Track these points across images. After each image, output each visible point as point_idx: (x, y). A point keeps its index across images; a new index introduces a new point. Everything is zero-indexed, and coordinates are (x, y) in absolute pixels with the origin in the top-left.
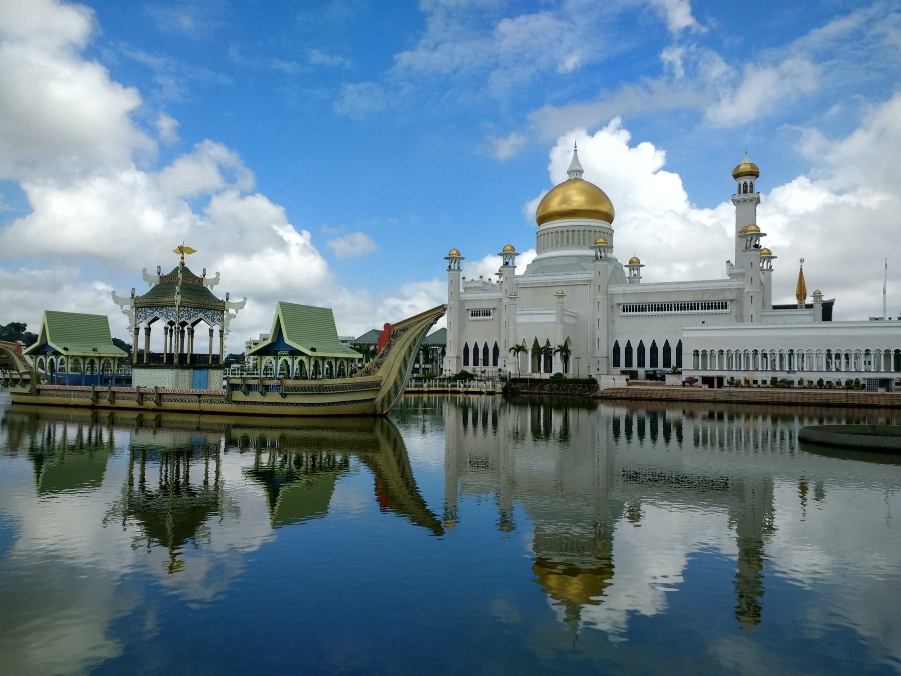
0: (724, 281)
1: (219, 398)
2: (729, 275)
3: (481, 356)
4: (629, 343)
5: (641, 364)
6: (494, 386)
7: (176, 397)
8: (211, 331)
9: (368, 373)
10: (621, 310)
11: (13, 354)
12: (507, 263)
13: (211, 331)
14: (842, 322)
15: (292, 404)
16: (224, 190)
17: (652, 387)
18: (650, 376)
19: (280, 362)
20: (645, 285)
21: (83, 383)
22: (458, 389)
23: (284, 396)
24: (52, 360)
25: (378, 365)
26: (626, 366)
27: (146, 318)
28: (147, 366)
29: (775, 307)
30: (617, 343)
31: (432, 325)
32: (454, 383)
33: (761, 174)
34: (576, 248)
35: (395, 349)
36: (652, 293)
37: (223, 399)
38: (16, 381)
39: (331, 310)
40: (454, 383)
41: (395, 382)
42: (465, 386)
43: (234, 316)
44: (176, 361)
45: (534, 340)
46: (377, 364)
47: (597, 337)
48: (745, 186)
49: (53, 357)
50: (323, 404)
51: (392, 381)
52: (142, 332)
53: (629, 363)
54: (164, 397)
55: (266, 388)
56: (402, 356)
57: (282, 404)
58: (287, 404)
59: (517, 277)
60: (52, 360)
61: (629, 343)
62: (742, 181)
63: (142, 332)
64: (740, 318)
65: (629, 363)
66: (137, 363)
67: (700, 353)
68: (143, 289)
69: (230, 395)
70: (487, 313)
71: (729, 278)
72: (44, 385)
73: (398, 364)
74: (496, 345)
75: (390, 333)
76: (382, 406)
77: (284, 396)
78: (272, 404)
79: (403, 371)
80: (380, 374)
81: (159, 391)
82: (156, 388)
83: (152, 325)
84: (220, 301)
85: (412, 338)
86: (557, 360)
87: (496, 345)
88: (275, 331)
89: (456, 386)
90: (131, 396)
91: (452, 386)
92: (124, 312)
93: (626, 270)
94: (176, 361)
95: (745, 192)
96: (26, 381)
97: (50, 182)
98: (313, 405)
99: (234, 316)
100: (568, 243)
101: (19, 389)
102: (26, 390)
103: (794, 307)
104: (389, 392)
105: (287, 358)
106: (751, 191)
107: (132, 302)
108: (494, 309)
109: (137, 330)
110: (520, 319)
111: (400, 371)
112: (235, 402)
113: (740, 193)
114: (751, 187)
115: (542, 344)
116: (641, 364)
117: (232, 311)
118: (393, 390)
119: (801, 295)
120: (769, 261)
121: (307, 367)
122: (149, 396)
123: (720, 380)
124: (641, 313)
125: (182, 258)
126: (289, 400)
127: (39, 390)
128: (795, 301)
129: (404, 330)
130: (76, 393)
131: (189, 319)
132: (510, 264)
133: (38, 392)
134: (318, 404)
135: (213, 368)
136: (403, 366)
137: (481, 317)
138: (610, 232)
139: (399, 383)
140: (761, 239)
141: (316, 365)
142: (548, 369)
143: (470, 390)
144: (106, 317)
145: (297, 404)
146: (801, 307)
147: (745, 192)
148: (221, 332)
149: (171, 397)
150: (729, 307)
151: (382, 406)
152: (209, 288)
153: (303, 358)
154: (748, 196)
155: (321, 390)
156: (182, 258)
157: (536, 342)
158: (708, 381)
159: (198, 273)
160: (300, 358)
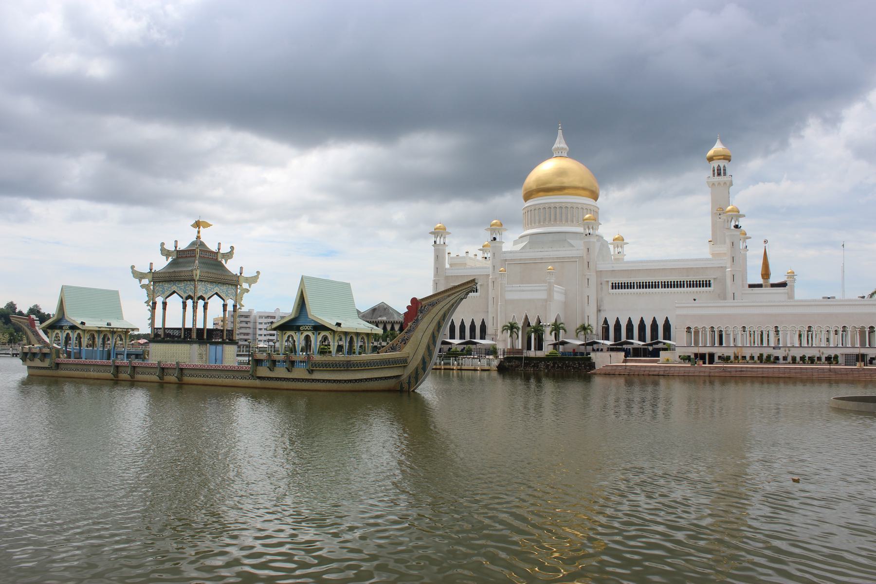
0: (707, 259)
1: (242, 374)
2: (712, 254)
4: (630, 321)
6: (489, 364)
7: (198, 372)
9: (393, 349)
11: (26, 328)
12: (495, 239)
13: (225, 306)
14: (801, 301)
15: (318, 380)
20: (628, 262)
22: (451, 367)
23: (311, 372)
24: (68, 334)
25: (405, 341)
27: (163, 293)
28: (163, 341)
29: (751, 286)
31: (462, 299)
32: (446, 361)
33: (732, 159)
34: (553, 225)
35: (422, 325)
36: (654, 270)
37: (246, 374)
38: (34, 355)
39: (117, 292)
40: (446, 361)
42: (458, 365)
43: (247, 291)
45: (524, 317)
46: (403, 340)
48: (719, 170)
49: (69, 332)
50: (350, 381)
51: (420, 357)
52: (159, 306)
54: (185, 372)
55: (274, 362)
57: (308, 380)
58: (313, 380)
59: (505, 252)
60: (68, 334)
62: (715, 164)
63: (159, 306)
64: (723, 296)
66: (185, 338)
67: (693, 330)
68: (161, 263)
69: (255, 371)
71: (710, 257)
72: (63, 358)
73: (425, 341)
74: (483, 322)
75: (417, 308)
76: (409, 383)
77: (311, 372)
78: (298, 380)
79: (432, 347)
80: (406, 351)
81: (162, 366)
82: (159, 363)
83: (168, 300)
84: (233, 276)
85: (441, 313)
87: (483, 322)
89: (449, 364)
90: (152, 371)
91: (445, 364)
92: (143, 286)
93: (611, 247)
94: (194, 335)
95: (719, 174)
96: (45, 356)
99: (247, 291)
100: (555, 220)
101: (37, 363)
102: (46, 364)
103: (760, 286)
104: (417, 369)
105: (310, 333)
106: (725, 174)
107: (151, 276)
109: (154, 304)
110: (509, 296)
111: (428, 347)
112: (259, 378)
113: (714, 174)
114: (725, 170)
115: (533, 323)
117: (245, 286)
119: (766, 274)
120: (744, 241)
122: (170, 371)
123: (712, 356)
125: (199, 232)
126: (316, 376)
127: (58, 365)
128: (760, 281)
129: (433, 305)
130: (96, 368)
131: (206, 293)
132: (498, 240)
133: (58, 365)
134: (345, 381)
135: (227, 343)
138: (596, 209)
139: (427, 359)
140: (740, 219)
141: (351, 342)
142: (540, 347)
143: (463, 367)
144: (349, 284)
145: (324, 380)
146: (766, 286)
147: (719, 174)
149: (193, 372)
151: (409, 383)
152: (223, 262)
154: (722, 178)
155: (348, 366)
156: (199, 232)
157: (526, 318)
159: (213, 248)
160: (323, 333)
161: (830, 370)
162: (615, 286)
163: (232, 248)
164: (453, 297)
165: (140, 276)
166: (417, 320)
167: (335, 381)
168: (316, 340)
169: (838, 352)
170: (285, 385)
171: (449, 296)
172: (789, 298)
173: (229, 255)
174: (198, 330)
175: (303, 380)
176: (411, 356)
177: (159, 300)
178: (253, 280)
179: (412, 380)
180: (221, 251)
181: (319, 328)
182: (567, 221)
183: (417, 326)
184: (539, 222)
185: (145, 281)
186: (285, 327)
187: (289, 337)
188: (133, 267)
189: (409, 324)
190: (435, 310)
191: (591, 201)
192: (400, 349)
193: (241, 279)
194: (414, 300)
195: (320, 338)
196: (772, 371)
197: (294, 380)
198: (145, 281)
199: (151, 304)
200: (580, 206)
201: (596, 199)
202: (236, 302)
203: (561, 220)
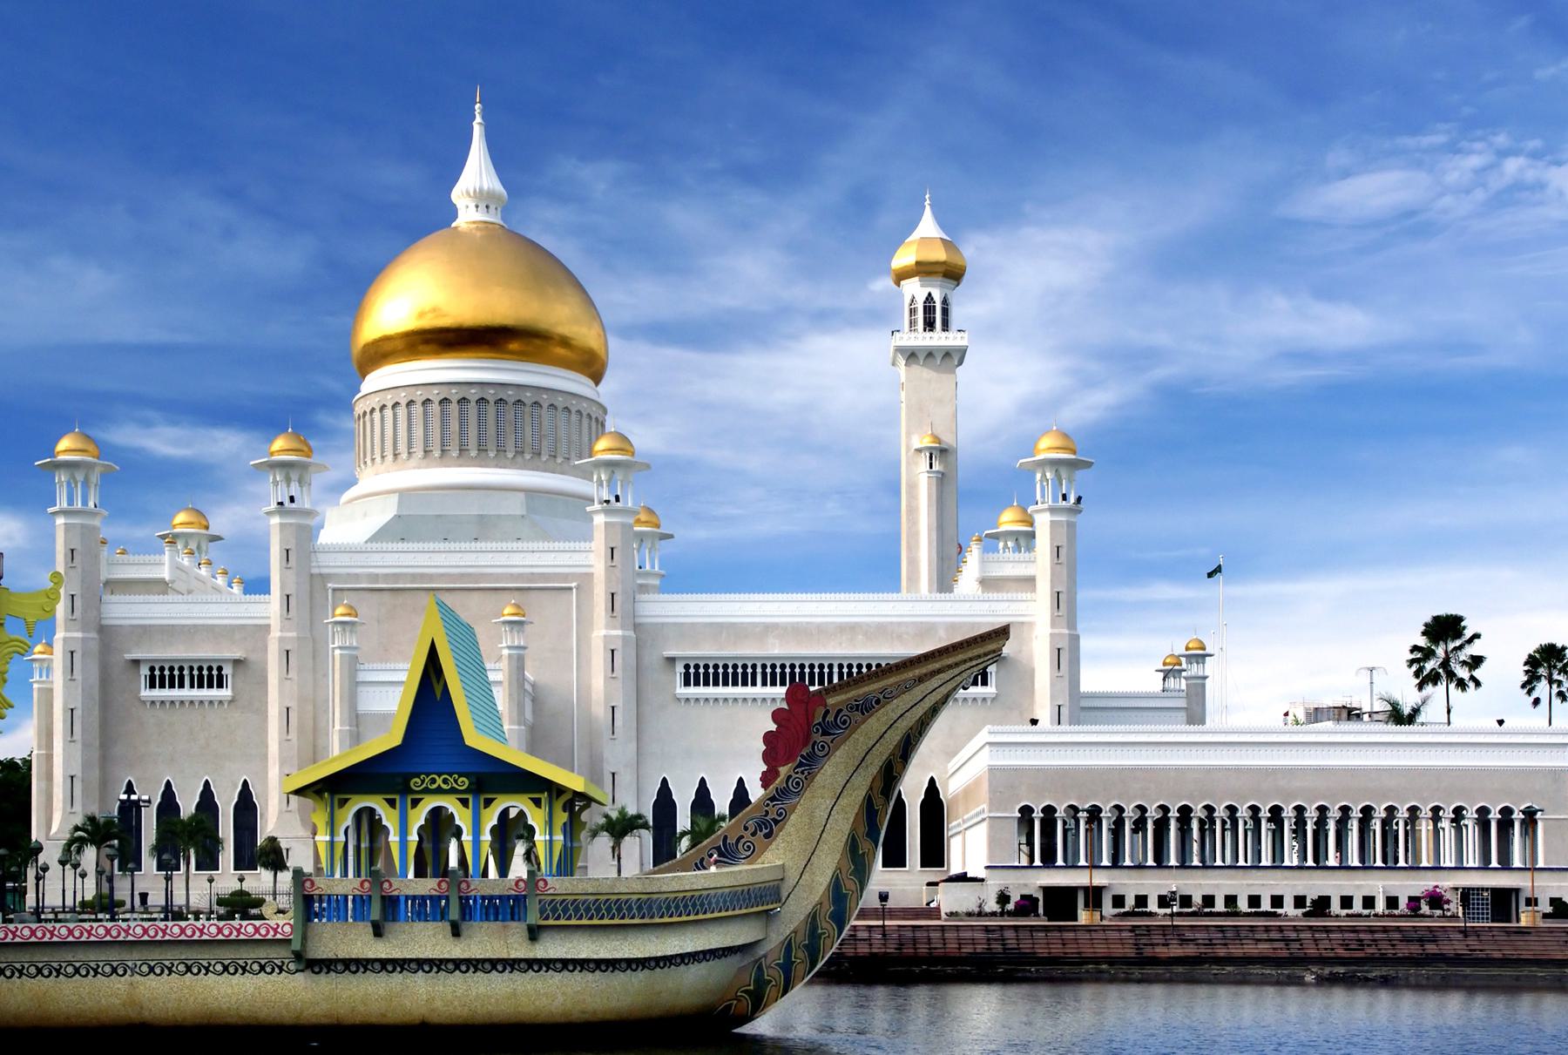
10: (679, 679)
19: (418, 817)
23: (534, 934)
30: (665, 787)
34: (512, 464)
35: (831, 772)
39: (1460, 619)
46: (761, 824)
47: (608, 769)
55: (391, 905)
70: (210, 676)
74: (245, 795)
75: (809, 717)
79: (865, 845)
85: (895, 737)
87: (245, 795)
97: (1338, 157)
104: (813, 918)
105: (451, 804)
108: (237, 663)
113: (912, 323)
114: (945, 312)
118: (829, 908)
121: (394, 838)
124: (740, 690)
129: (866, 707)
136: (862, 829)
137: (187, 693)
138: (595, 412)
139: (849, 885)
147: (929, 325)
150: (992, 679)
162: (698, 674)
164: (935, 682)
168: (474, 827)
169: (1446, 882)
171: (921, 680)
172: (1190, 721)
175: (511, 964)
176: (792, 877)
179: (799, 956)
181: (492, 777)
182: (520, 452)
183: (811, 777)
186: (378, 776)
187: (358, 815)
190: (874, 724)
191: (576, 383)
192: (753, 853)
200: (528, 397)
201: (597, 378)
203: (501, 450)
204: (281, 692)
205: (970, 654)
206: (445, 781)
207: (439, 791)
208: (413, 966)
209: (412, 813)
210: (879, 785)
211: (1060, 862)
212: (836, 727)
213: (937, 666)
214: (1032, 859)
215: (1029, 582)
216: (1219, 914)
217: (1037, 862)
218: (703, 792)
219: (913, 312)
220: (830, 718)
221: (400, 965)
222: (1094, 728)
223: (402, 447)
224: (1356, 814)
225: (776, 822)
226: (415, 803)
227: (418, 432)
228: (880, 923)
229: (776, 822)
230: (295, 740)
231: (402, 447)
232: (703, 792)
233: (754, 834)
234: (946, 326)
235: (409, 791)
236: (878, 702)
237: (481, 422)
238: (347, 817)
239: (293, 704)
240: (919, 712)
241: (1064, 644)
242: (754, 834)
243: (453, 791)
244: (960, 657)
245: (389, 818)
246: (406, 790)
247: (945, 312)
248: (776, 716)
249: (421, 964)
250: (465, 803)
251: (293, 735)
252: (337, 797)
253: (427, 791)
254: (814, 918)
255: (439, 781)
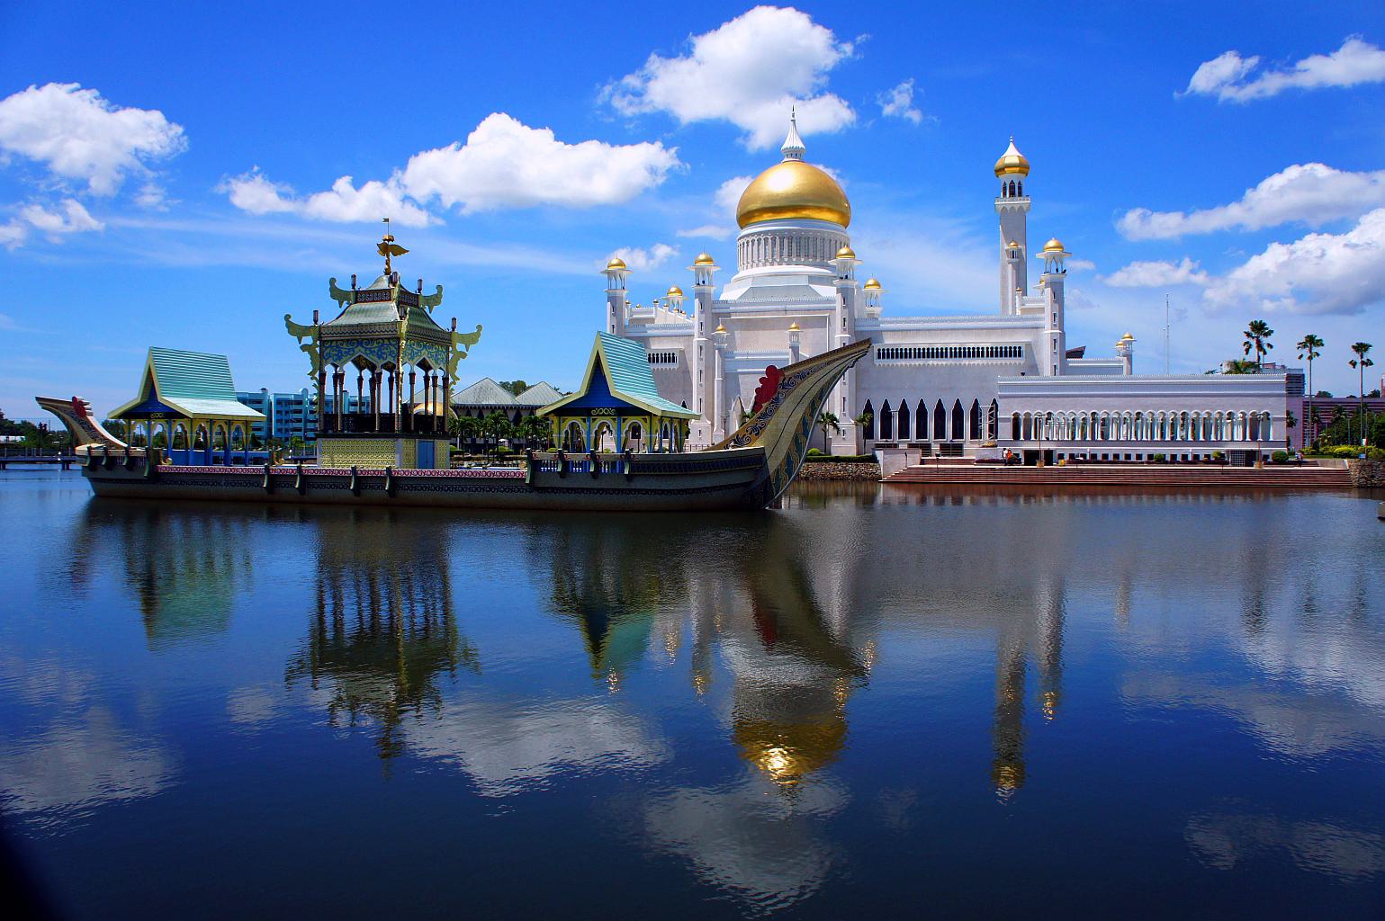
3: (896, 422)
4: (922, 405)
5: (940, 432)
8: (360, 380)
16: (1217, 86)
17: (950, 465)
18: (945, 449)
19: (595, 427)
21: (1043, 454)
26: (918, 437)
35: (786, 405)
41: (788, 456)
44: (397, 426)
46: (754, 429)
51: (782, 456)
53: (922, 432)
56: (798, 415)
57: (590, 490)
61: (922, 405)
65: (922, 432)
73: (792, 428)
75: (776, 380)
85: (816, 389)
86: (257, 433)
88: (146, 385)
92: (304, 348)
94: (397, 426)
98: (670, 492)
99: (463, 355)
109: (323, 375)
113: (1005, 194)
114: (1020, 188)
116: (940, 432)
117: (460, 347)
129: (803, 376)
147: (1012, 194)
148: (445, 380)
152: (427, 310)
153: (638, 420)
158: (1031, 457)
160: (631, 420)
161: (1223, 472)
163: (439, 288)
164: (836, 364)
165: (295, 330)
166: (777, 399)
167: (663, 491)
170: (583, 499)
171: (828, 363)
173: (435, 300)
174: (383, 416)
177: (330, 370)
178: (471, 339)
180: (424, 293)
183: (777, 408)
184: (790, 255)
185: (308, 340)
188: (287, 317)
189: (764, 405)
192: (750, 441)
193: (454, 337)
194: (771, 370)
195: (566, 426)
196: (1093, 482)
197: (569, 490)
198: (308, 340)
199: (317, 375)
202: (447, 373)
204: (698, 364)
205: (854, 350)
206: (606, 411)
207: (603, 415)
208: (611, 492)
209: (592, 425)
210: (809, 411)
211: (1033, 438)
212: (789, 385)
213: (836, 357)
214: (1244, 436)
215: (1042, 310)
216: (1133, 463)
217: (1248, 439)
218: (886, 405)
219: (1005, 189)
220: (786, 381)
221: (639, 491)
222: (1094, 376)
223: (755, 259)
224: (1179, 416)
225: (761, 428)
226: (594, 420)
227: (762, 251)
228: (939, 466)
229: (761, 428)
230: (847, 382)
231: (755, 259)
232: (886, 405)
233: (751, 433)
234: (1020, 194)
235: (590, 415)
236: (808, 374)
237: (790, 246)
238: (626, 427)
239: (703, 369)
240: (827, 378)
241: (1057, 337)
242: (751, 433)
243: (609, 415)
244: (848, 353)
245: (583, 427)
246: (590, 415)
247: (1020, 188)
248: (762, 380)
249: (583, 490)
250: (614, 420)
251: (703, 382)
252: (562, 418)
253: (598, 415)
254: (778, 472)
255: (604, 411)
